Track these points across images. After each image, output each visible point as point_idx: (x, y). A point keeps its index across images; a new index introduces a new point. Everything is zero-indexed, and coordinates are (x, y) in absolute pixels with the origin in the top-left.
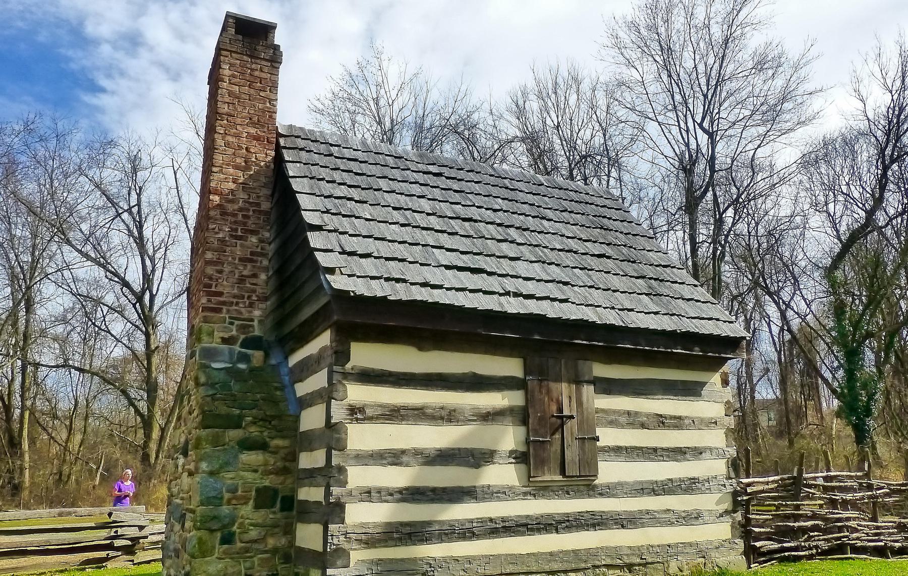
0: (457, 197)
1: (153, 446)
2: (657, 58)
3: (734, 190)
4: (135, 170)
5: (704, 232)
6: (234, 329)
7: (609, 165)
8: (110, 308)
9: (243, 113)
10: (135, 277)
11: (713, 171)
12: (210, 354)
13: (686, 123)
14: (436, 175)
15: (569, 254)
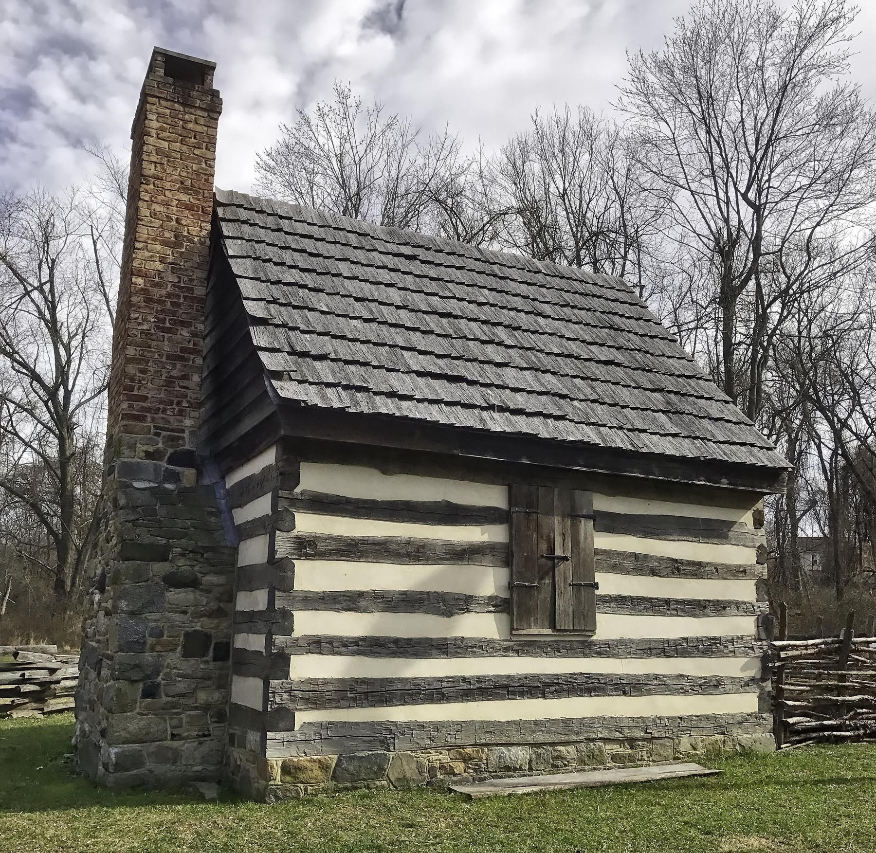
0: (433, 287)
1: (69, 571)
2: (694, 109)
3: (783, 278)
4: (46, 240)
5: (741, 331)
6: (161, 442)
7: (625, 244)
8: (18, 405)
9: (174, 174)
10: (46, 368)
11: (757, 254)
12: (132, 471)
13: (726, 193)
14: (408, 257)
15: (568, 360)
